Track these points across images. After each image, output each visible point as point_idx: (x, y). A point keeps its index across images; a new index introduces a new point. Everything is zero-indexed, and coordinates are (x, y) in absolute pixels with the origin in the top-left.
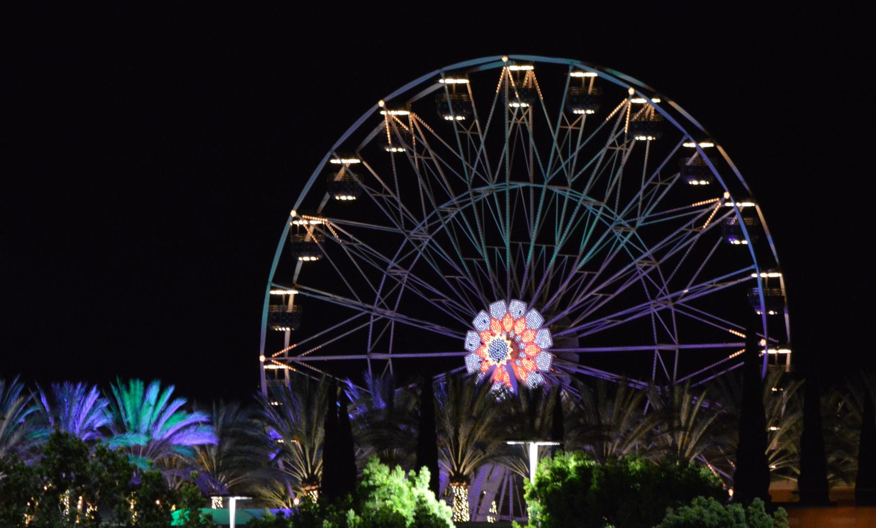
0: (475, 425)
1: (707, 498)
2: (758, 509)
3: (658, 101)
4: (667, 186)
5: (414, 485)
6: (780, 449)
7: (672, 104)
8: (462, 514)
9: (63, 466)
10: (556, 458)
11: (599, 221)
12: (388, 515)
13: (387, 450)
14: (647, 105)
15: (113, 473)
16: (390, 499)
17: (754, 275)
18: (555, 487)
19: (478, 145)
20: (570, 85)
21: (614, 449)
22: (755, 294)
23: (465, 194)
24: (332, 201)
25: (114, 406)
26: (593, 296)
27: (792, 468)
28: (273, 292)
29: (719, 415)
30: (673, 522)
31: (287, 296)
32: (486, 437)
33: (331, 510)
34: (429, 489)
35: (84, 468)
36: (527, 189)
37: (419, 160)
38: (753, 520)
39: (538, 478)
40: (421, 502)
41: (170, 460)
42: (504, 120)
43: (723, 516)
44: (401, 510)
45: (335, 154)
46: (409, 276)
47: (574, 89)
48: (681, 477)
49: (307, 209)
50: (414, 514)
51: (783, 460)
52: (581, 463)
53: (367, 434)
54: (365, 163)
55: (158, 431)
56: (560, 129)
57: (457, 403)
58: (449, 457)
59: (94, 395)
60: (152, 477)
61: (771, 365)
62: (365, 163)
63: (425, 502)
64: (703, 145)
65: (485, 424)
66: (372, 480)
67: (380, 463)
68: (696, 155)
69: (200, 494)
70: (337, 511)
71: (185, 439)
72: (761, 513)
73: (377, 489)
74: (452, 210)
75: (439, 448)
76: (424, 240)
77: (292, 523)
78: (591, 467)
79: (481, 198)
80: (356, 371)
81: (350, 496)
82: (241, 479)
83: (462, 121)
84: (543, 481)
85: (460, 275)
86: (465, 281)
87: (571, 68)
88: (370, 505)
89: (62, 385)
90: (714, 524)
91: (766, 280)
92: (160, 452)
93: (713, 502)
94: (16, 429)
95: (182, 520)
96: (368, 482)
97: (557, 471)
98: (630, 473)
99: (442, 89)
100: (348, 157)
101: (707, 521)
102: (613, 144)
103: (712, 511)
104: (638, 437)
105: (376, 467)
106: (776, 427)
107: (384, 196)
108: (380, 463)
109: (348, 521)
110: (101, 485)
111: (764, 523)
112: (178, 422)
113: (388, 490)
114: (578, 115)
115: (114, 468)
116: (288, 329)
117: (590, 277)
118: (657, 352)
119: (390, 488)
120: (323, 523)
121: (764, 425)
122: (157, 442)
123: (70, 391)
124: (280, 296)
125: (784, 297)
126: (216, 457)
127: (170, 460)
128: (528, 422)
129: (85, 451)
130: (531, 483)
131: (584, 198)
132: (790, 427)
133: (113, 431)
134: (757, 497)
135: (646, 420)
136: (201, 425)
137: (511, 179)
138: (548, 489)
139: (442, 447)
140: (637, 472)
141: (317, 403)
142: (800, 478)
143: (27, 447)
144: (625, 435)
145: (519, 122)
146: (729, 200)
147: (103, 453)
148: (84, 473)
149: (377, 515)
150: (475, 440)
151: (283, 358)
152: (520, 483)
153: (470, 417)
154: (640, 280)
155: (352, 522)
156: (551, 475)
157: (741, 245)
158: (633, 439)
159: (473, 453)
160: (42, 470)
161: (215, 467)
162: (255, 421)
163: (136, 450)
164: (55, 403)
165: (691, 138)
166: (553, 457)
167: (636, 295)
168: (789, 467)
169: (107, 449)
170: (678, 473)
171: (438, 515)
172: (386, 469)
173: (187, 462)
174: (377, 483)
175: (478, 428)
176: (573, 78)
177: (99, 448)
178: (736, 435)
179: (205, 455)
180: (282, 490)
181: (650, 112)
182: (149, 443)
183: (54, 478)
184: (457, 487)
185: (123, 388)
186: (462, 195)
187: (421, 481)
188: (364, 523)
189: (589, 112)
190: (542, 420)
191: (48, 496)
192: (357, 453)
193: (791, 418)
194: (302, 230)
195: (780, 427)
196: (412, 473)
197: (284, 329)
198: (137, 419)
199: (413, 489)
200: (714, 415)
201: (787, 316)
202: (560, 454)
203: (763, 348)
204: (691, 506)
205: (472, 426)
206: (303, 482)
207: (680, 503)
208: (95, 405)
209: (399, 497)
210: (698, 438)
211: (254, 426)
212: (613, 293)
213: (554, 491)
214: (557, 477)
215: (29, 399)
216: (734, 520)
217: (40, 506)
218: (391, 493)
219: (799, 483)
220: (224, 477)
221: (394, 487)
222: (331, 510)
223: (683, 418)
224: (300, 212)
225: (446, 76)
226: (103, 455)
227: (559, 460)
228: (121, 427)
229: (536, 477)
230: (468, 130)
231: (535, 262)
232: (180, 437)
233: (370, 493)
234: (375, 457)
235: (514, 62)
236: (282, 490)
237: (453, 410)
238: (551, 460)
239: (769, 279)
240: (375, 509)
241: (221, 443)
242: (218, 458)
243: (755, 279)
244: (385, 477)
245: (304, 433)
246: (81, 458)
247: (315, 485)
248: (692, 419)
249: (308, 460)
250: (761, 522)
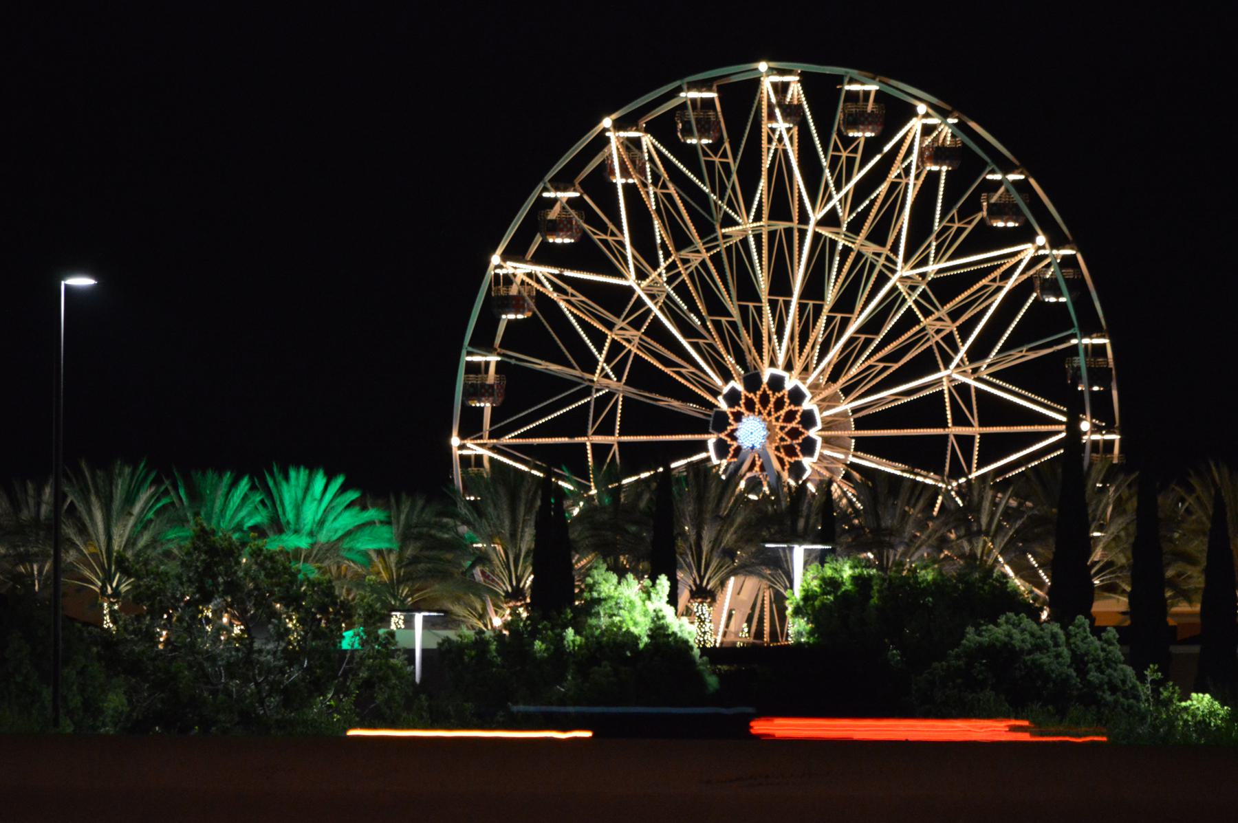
0: (723, 526)
1: (1017, 615)
2: (1081, 629)
3: (956, 121)
4: (965, 229)
5: (649, 598)
6: (1105, 560)
7: (973, 125)
8: (706, 638)
9: (208, 571)
10: (826, 565)
11: (881, 271)
12: (616, 634)
13: (612, 557)
14: (942, 127)
15: (272, 578)
16: (618, 615)
17: (1074, 341)
18: (826, 601)
19: (729, 177)
20: (845, 101)
21: (897, 558)
22: (1075, 365)
23: (712, 236)
24: (544, 244)
25: (271, 500)
26: (870, 367)
27: (1120, 584)
28: (469, 359)
29: (1029, 517)
30: (975, 644)
31: (487, 364)
32: (736, 542)
33: (545, 628)
34: (668, 602)
35: (235, 572)
36: (789, 232)
37: (655, 193)
38: (1074, 643)
39: (804, 590)
40: (658, 617)
41: (339, 568)
42: (761, 144)
43: (1039, 638)
44: (633, 629)
45: (549, 186)
46: (640, 339)
47: (849, 105)
48: (984, 590)
49: (516, 252)
50: (649, 633)
51: (1109, 573)
52: (858, 571)
53: (587, 537)
54: (586, 197)
55: (324, 532)
56: (832, 156)
57: (700, 499)
58: (689, 566)
59: (244, 485)
60: (320, 584)
61: (1094, 455)
62: (586, 197)
63: (663, 617)
64: (1012, 177)
65: (736, 525)
66: (596, 591)
67: (607, 570)
68: (1002, 189)
69: (378, 605)
70: (552, 629)
71: (358, 542)
72: (1085, 635)
73: (603, 603)
74: (699, 254)
75: (678, 556)
76: (660, 293)
77: (495, 643)
78: (870, 577)
79: (732, 242)
80: (572, 459)
81: (569, 611)
82: (427, 593)
83: (708, 145)
84: (810, 593)
85: (704, 338)
86: (710, 345)
87: (846, 80)
88: (593, 621)
89: (204, 474)
90: (1026, 648)
91: (1090, 348)
92: (327, 558)
93: (1026, 620)
94: (145, 527)
95: (358, 638)
96: (591, 594)
97: (828, 581)
98: (920, 584)
99: (683, 106)
100: (565, 190)
101: (1017, 644)
102: (899, 176)
103: (1023, 631)
104: (927, 544)
105: (602, 575)
106: (1101, 532)
107: (610, 239)
108: (607, 570)
109: (566, 642)
110: (256, 593)
111: (1089, 646)
112: (348, 520)
113: (617, 603)
114: (855, 139)
115: (272, 571)
116: (488, 405)
117: (868, 342)
118: (952, 438)
119: (619, 601)
120: (533, 644)
121: (1087, 531)
122: (322, 545)
123: (214, 482)
124: (479, 364)
125: (1111, 369)
126: (396, 564)
127: (339, 568)
128: (789, 523)
129: (236, 551)
130: (796, 595)
131: (860, 243)
132: (1118, 532)
133: (268, 532)
134: (1083, 615)
135: (937, 522)
136: (378, 525)
137: (770, 218)
138: (817, 603)
139: (681, 554)
140: (928, 583)
141: (523, 496)
142: (1131, 596)
143: (159, 550)
144: (911, 541)
145: (780, 147)
146: (1043, 247)
147: (259, 552)
148: (235, 578)
149: (602, 634)
150: (723, 545)
151: (482, 441)
152: (779, 600)
153: (717, 517)
154: (931, 346)
155: (571, 644)
156: (820, 586)
157: (1057, 303)
158: (920, 546)
159: (719, 562)
160: (181, 575)
161: (395, 577)
162: (445, 520)
163: (297, 553)
164: (196, 496)
165: (996, 169)
166: (822, 563)
167: (926, 364)
168: (1117, 584)
169: (264, 548)
170: (980, 585)
171: (679, 634)
172: (614, 578)
173: (360, 570)
174: (603, 595)
175: (727, 531)
176: (848, 92)
177: (254, 548)
178: (1051, 541)
179: (381, 560)
180: (479, 607)
181: (945, 137)
182: (313, 545)
183: (197, 584)
184: (699, 603)
185: (280, 478)
186: (709, 238)
187: (657, 593)
188: (586, 643)
189: (868, 134)
190: (807, 523)
191: (189, 607)
192: (574, 561)
193: (1120, 521)
194: (508, 280)
195: (1106, 532)
196: (647, 582)
197: (482, 405)
198: (298, 516)
199: (647, 602)
200: (1023, 517)
201: (1115, 393)
202: (832, 560)
203: (1085, 433)
204: (997, 625)
205: (719, 528)
206: (505, 597)
207: (982, 622)
208: (245, 498)
209: (629, 612)
210: (1002, 545)
211: (443, 527)
212: (896, 361)
213: (823, 605)
214: (828, 589)
215: (163, 488)
216: (1051, 642)
217: (180, 619)
218: (620, 608)
219: (1131, 603)
220: (407, 590)
221: (623, 600)
222: (545, 628)
223: (984, 520)
224: (506, 256)
225: (689, 89)
226: (259, 556)
227: (830, 568)
228: (278, 526)
229: (801, 588)
230: (716, 155)
231: (800, 319)
232: (353, 540)
233: (593, 607)
234: (601, 562)
235: (775, 72)
236: (479, 607)
237: (694, 509)
238: (820, 567)
239: (1094, 346)
240: (600, 627)
241: (402, 549)
242: (399, 566)
243: (1076, 346)
244: (613, 588)
245: (508, 535)
246: (231, 559)
247: (520, 601)
248: (996, 521)
249: (512, 569)
250: (1085, 646)
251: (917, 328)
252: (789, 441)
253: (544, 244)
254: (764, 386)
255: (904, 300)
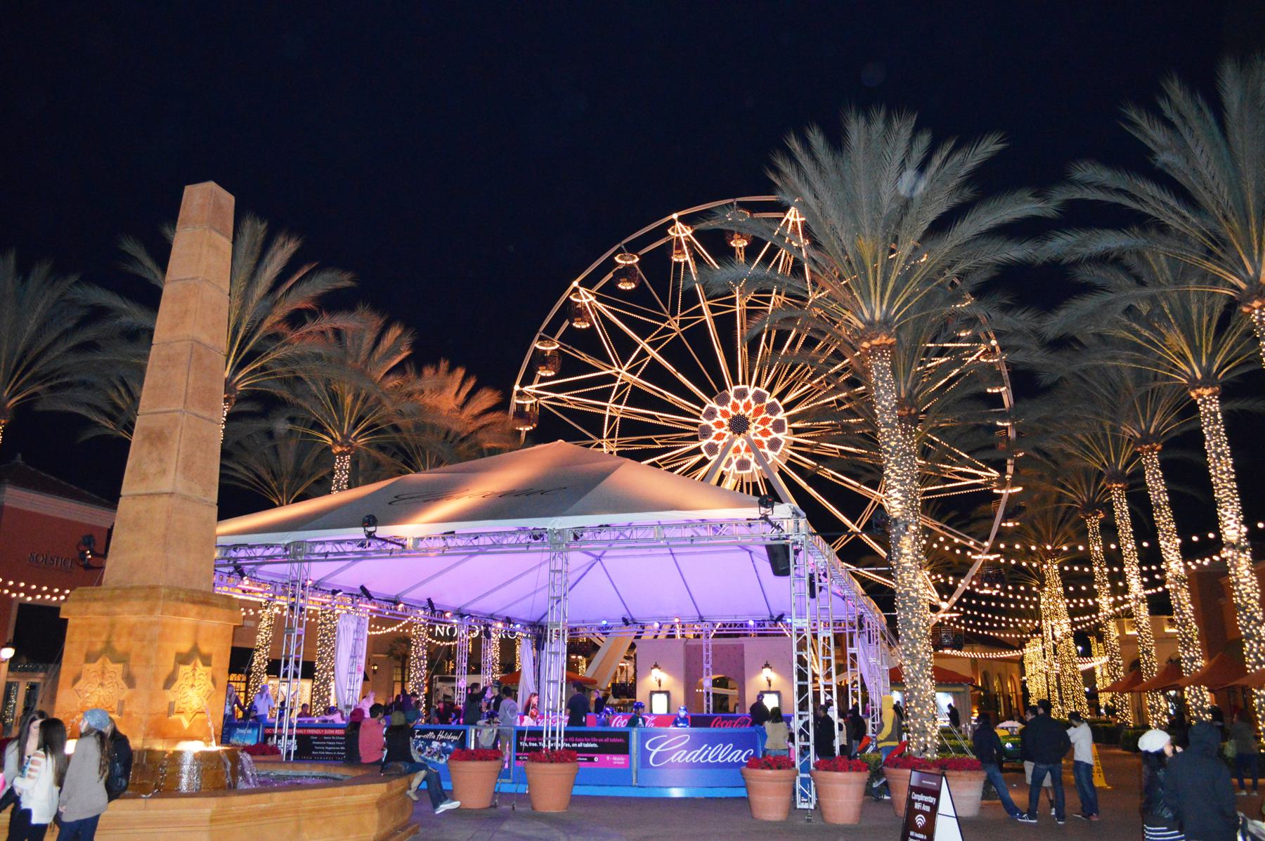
252: (762, 428)
253: (570, 327)
254: (765, 404)
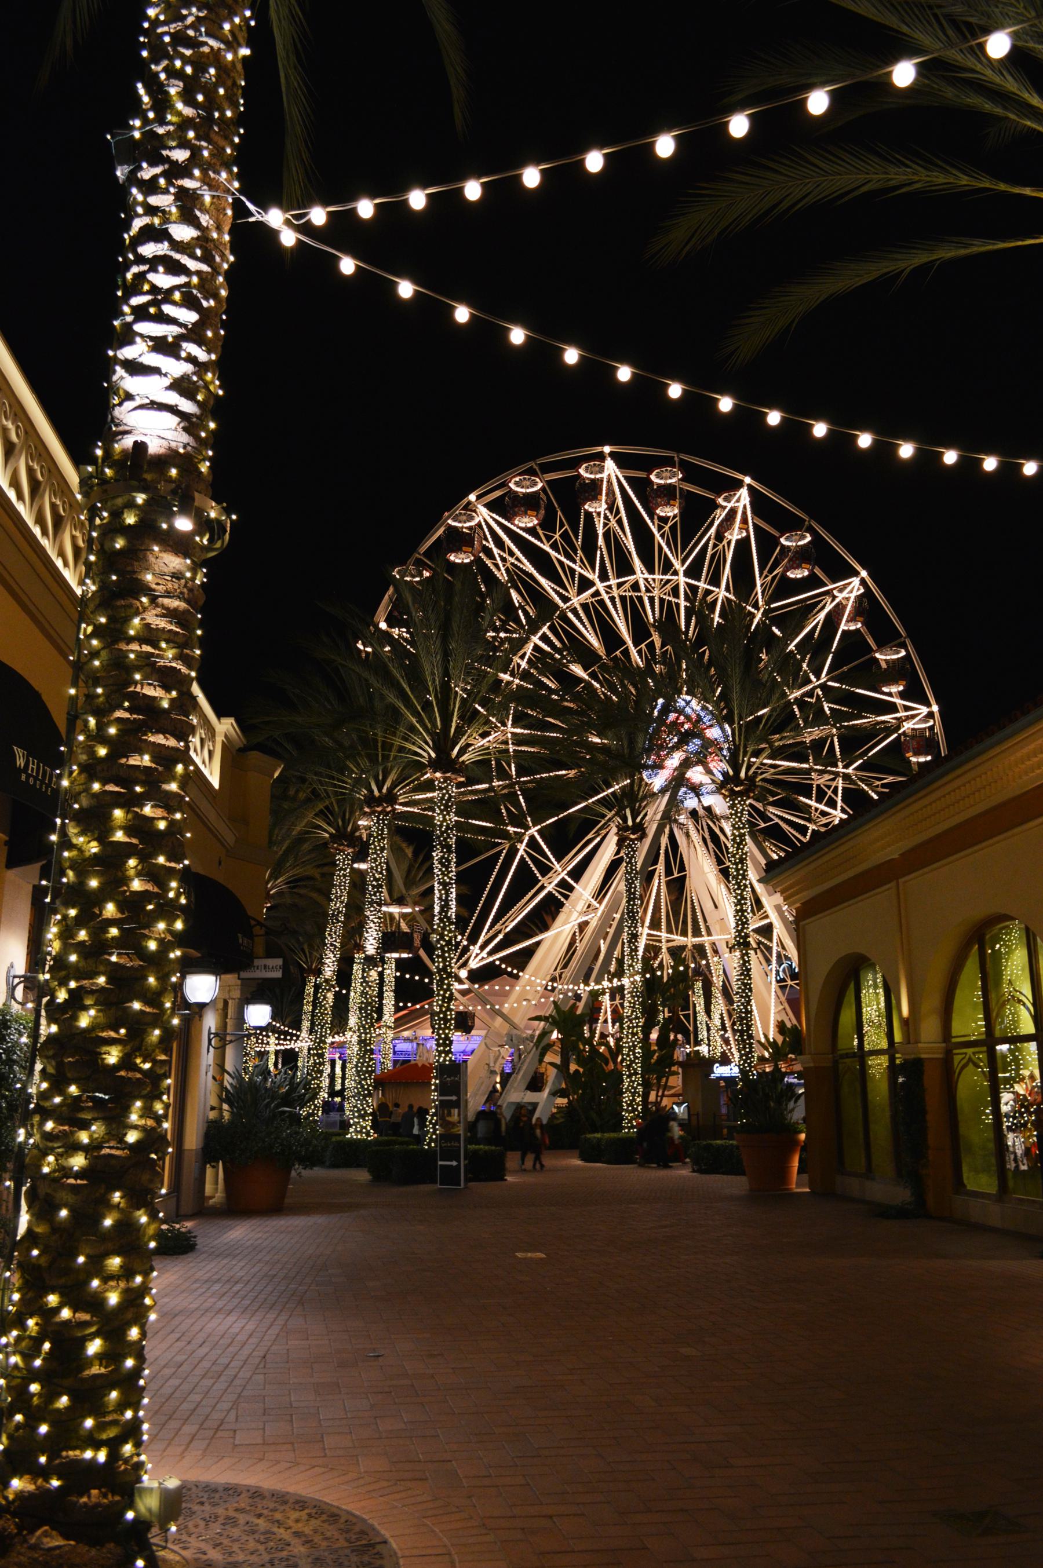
102: (605, 525)
145: (508, 565)
251: (569, 869)
255: (678, 605)
